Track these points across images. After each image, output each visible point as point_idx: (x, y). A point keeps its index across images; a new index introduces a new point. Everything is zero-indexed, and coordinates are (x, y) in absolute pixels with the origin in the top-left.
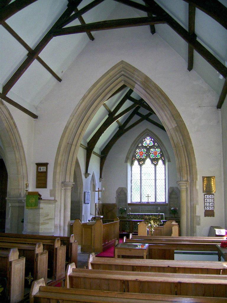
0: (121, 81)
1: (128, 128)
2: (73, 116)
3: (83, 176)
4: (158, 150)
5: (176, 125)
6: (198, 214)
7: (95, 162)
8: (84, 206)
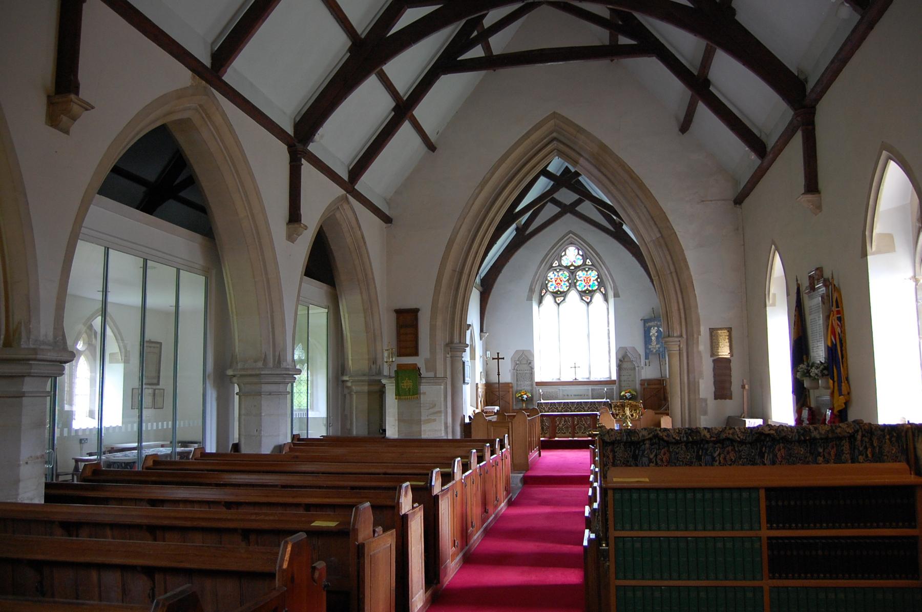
4: (593, 274)
5: (658, 235)
6: (702, 395)
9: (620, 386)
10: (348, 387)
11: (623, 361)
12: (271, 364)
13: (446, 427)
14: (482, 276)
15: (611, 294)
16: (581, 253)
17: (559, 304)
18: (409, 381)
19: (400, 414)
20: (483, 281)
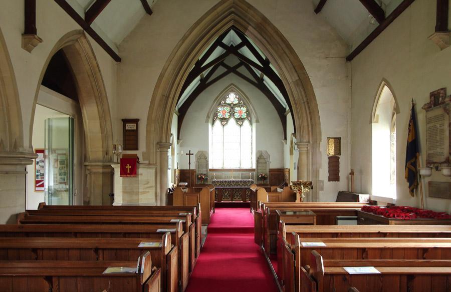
1: (254, 77)
4: (244, 109)
5: (297, 78)
9: (258, 172)
10: (88, 170)
11: (261, 158)
12: (8, 149)
13: (156, 196)
14: (179, 107)
15: (254, 120)
16: (237, 97)
17: (224, 125)
18: (130, 167)
19: (124, 188)
20: (180, 110)
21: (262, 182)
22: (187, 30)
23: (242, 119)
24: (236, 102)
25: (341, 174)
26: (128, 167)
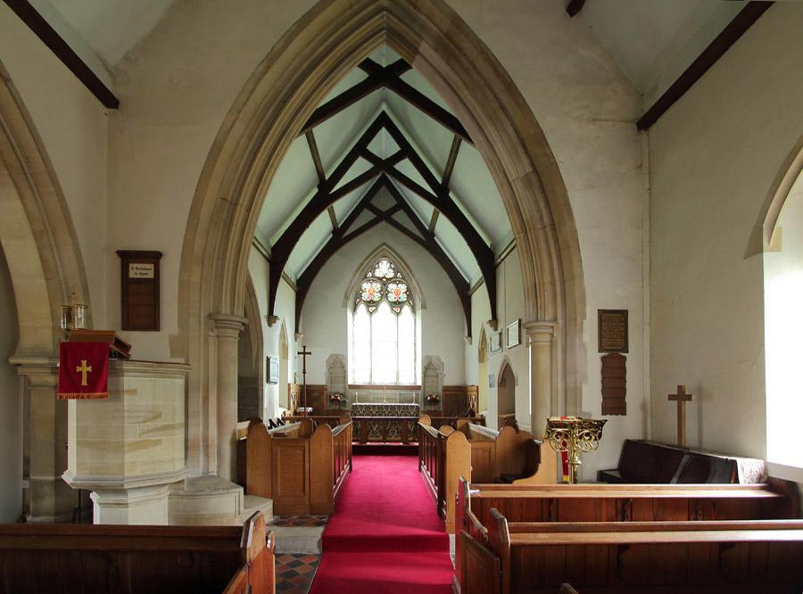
0: (380, 31)
2: (239, 112)
3: (264, 322)
4: (403, 287)
5: (529, 169)
7: (286, 295)
8: (266, 387)
9: (425, 391)
11: (429, 368)
15: (418, 305)
17: (371, 313)
21: (432, 408)
22: (282, 33)
23: (400, 303)
24: (391, 274)
25: (629, 399)
26: (85, 369)
